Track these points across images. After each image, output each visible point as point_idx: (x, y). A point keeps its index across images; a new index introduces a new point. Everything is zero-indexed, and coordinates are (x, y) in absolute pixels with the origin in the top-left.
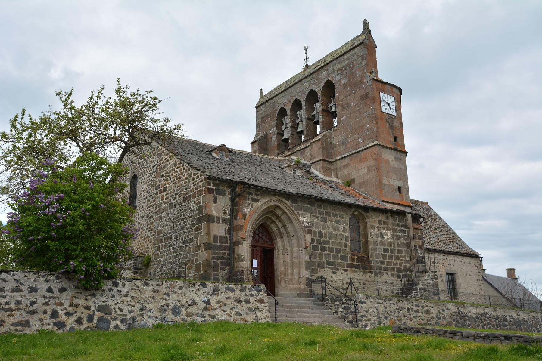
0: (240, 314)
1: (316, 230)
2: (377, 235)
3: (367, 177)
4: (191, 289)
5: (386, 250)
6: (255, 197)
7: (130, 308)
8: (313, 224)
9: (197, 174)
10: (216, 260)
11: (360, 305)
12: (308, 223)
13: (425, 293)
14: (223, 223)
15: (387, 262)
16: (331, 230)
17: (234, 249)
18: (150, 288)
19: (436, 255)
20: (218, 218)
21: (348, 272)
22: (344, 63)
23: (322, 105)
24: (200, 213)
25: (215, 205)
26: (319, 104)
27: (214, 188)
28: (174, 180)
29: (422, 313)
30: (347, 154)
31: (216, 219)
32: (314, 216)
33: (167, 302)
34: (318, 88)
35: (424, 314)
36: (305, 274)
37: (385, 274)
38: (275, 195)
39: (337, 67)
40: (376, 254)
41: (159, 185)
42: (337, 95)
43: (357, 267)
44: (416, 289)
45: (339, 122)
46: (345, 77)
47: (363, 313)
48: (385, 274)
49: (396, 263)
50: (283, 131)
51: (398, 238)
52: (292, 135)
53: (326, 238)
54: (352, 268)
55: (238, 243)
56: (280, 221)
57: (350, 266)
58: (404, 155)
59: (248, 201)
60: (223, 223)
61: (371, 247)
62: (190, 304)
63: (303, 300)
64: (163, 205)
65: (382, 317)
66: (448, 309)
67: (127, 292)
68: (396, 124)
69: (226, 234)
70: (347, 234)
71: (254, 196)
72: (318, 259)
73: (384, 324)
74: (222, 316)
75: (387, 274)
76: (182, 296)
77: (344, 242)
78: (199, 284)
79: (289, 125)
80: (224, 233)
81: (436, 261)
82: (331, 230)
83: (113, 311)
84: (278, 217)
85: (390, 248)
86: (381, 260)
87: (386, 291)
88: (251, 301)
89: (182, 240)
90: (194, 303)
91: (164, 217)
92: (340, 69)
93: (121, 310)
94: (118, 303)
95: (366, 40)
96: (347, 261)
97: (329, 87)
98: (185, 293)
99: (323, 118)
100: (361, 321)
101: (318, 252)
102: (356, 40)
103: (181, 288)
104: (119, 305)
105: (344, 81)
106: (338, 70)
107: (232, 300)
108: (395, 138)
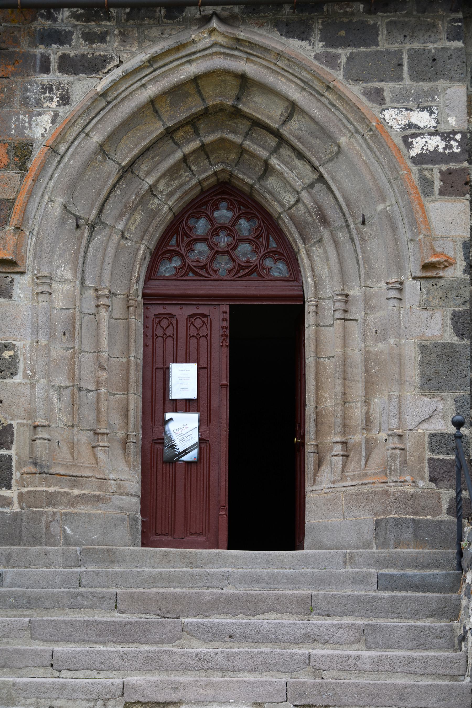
12: (447, 136)
59: (44, 78)
71: (77, 48)
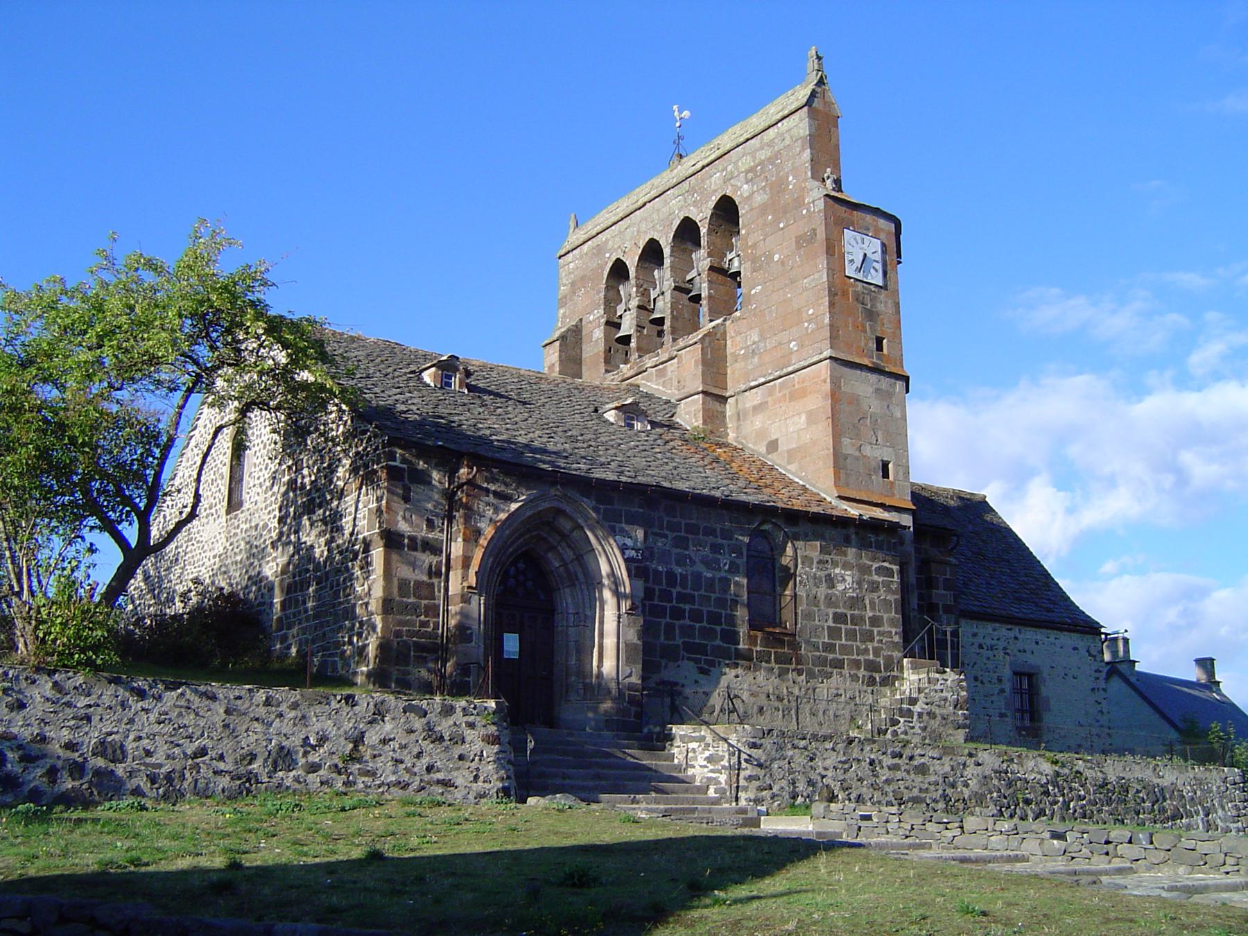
2: (817, 581)
3: (806, 438)
8: (652, 554)
12: (637, 551)
16: (700, 567)
19: (989, 627)
22: (762, 155)
23: (710, 255)
26: (703, 252)
30: (762, 380)
32: (656, 534)
34: (702, 215)
35: (913, 776)
38: (554, 483)
39: (746, 163)
50: (621, 317)
51: (874, 587)
52: (640, 327)
53: (684, 586)
56: (569, 546)
58: (900, 385)
79: (634, 303)
81: (989, 642)
82: (700, 567)
84: (564, 536)
88: (468, 739)
89: (332, 588)
92: (752, 170)
97: (727, 211)
99: (710, 289)
101: (663, 621)
103: (295, 706)
105: (759, 199)
106: (747, 172)
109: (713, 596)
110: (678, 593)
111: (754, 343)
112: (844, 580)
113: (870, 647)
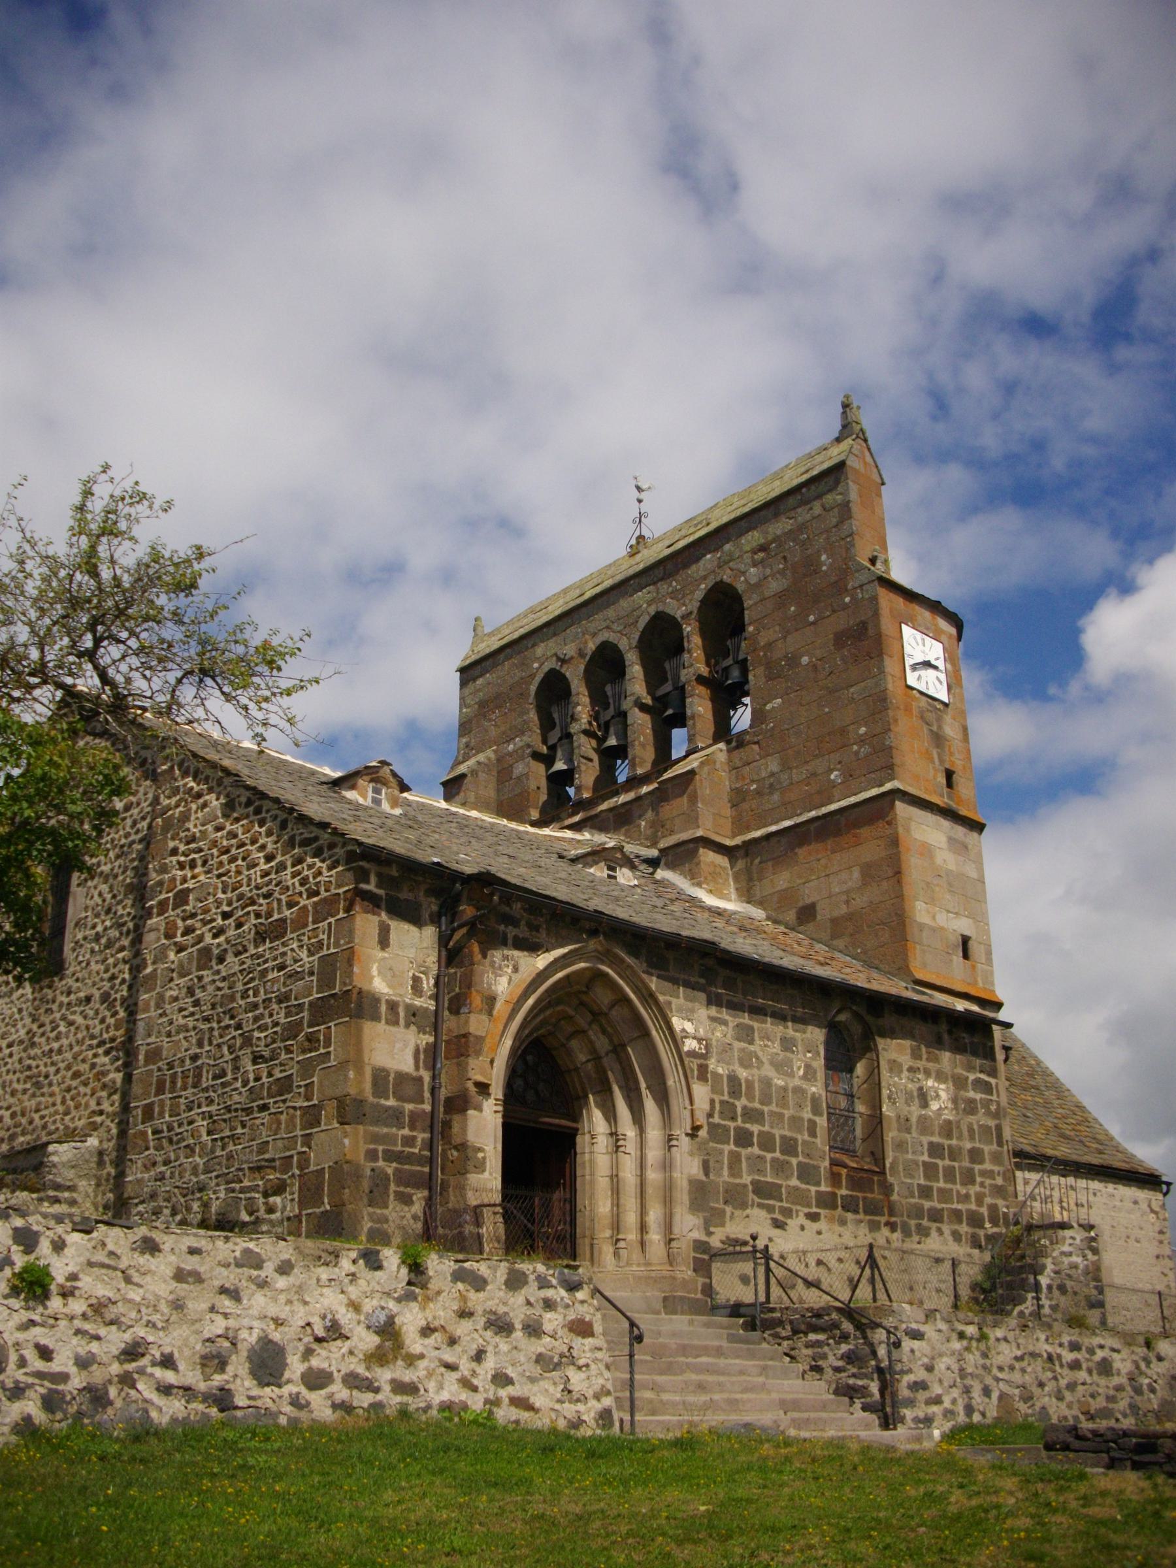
0: (509, 1381)
1: (720, 1071)
3: (860, 901)
4: (324, 1273)
5: (935, 1150)
6: (527, 934)
7: (83, 1347)
9: (316, 839)
10: (381, 1163)
11: (907, 1344)
12: (700, 1040)
13: (1063, 1299)
14: (407, 1026)
15: (940, 1190)
16: (768, 1071)
17: (447, 1125)
18: (162, 1265)
20: (393, 1006)
21: (822, 1225)
24: (326, 980)
25: (381, 954)
27: (381, 892)
28: (221, 864)
29: (1090, 1371)
31: (383, 1008)
33: (232, 1323)
35: (1095, 1377)
36: (689, 1226)
37: (934, 1233)
38: (594, 933)
40: (906, 1156)
41: (161, 883)
42: (751, 629)
43: (850, 1206)
44: (1037, 1287)
45: (758, 717)
46: (782, 573)
47: (920, 1375)
48: (934, 1233)
49: (967, 1196)
51: (971, 1108)
53: (751, 1098)
54: (835, 1207)
55: (459, 1104)
56: (604, 1032)
57: (827, 1201)
60: (407, 1026)
61: (891, 1135)
62: (321, 1333)
63: (691, 1322)
64: (172, 955)
65: (976, 1393)
66: (1160, 1359)
67: (73, 1277)
68: (950, 730)
69: (417, 1068)
70: (816, 1088)
72: (726, 1172)
73: (983, 1415)
74: (441, 1387)
75: (940, 1231)
76: (289, 1302)
77: (807, 1114)
78: (354, 1255)
80: (410, 1061)
82: (768, 1071)
83: (13, 1357)
85: (946, 1142)
86: (922, 1182)
87: (938, 1291)
88: (548, 1327)
90: (335, 1332)
91: (176, 999)
92: (763, 548)
93: (45, 1353)
94: (33, 1323)
95: (852, 457)
96: (818, 1184)
98: (300, 1289)
100: (911, 1403)
102: (819, 458)
104: (37, 1330)
106: (754, 552)
107: (481, 1321)
108: (949, 775)
109: (787, 1113)
110: (744, 1108)
111: (772, 774)
112: (938, 1096)
113: (972, 1192)
